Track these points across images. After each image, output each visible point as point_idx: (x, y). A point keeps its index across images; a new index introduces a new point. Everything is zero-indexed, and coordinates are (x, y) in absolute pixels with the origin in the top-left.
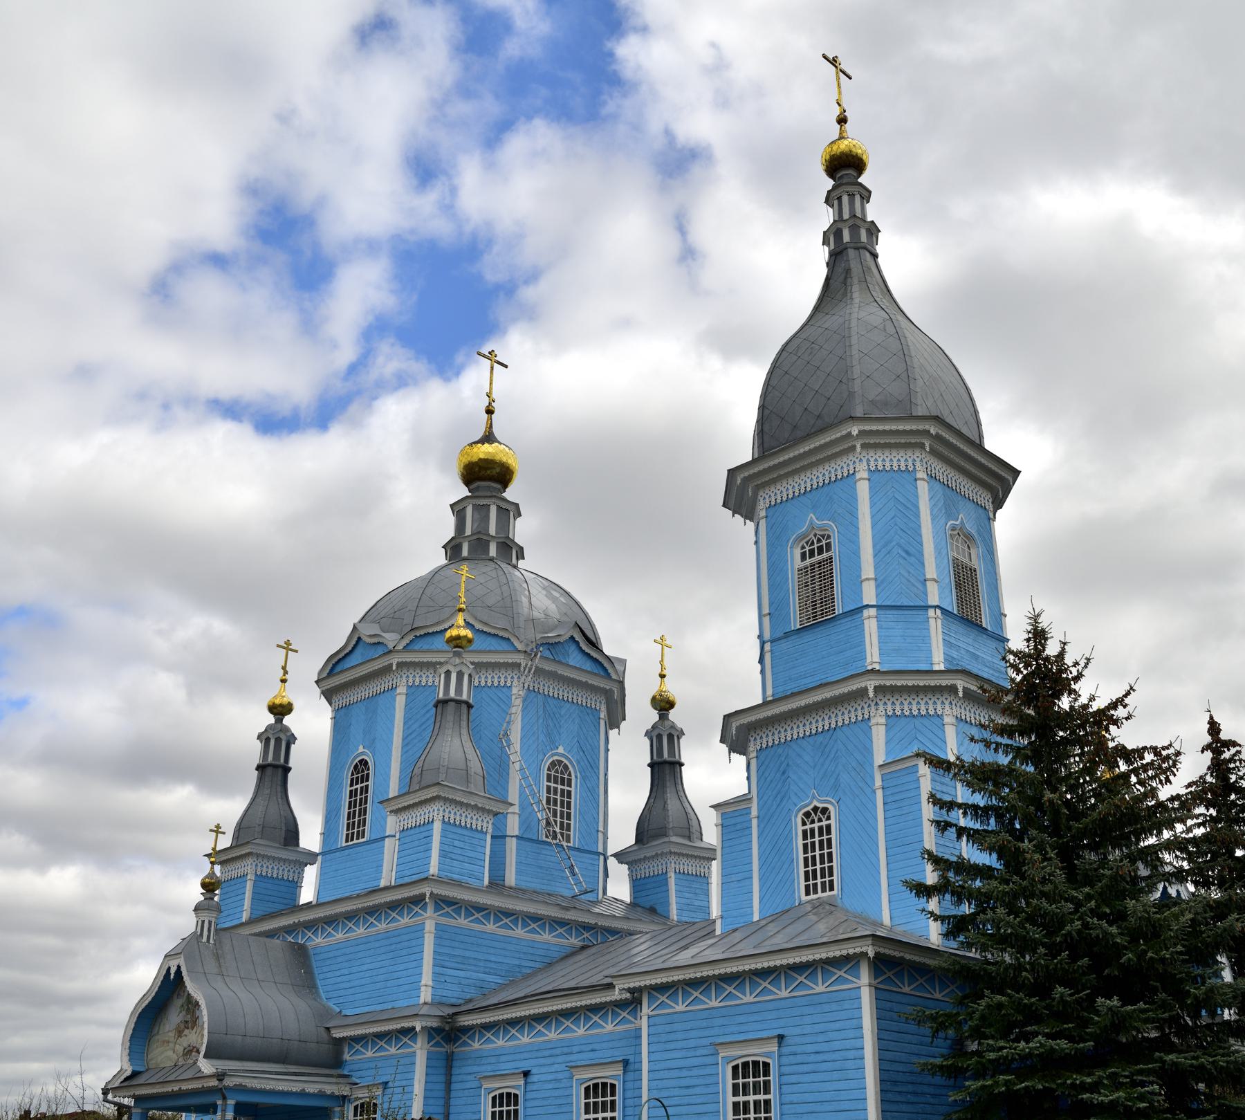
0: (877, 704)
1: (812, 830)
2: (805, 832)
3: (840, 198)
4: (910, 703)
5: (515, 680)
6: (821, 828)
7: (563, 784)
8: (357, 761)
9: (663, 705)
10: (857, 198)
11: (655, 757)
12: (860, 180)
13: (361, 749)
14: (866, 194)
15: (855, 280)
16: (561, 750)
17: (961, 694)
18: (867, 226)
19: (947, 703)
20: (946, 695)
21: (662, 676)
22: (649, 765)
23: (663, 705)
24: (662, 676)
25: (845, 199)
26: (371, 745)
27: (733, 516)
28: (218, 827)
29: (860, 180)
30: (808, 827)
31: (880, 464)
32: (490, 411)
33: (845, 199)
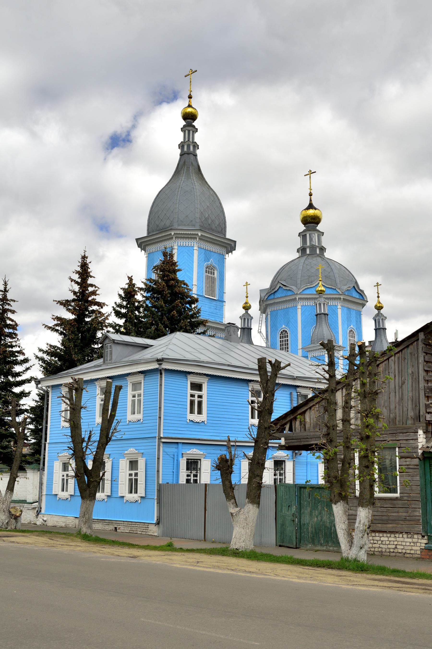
0: (299, 302)
1: (283, 340)
2: (281, 341)
3: (185, 131)
4: (335, 302)
5: (338, 303)
6: (285, 340)
7: (353, 338)
8: (282, 330)
9: (379, 308)
10: (191, 132)
11: (377, 327)
12: (193, 124)
13: (284, 326)
14: (195, 130)
15: (186, 167)
16: (352, 326)
17: (342, 300)
18: (193, 144)
19: (338, 302)
20: (338, 300)
21: (247, 297)
22: (375, 329)
23: (379, 308)
24: (247, 297)
25: (187, 132)
26: (287, 325)
27: (141, 251)
28: (377, 283)
29: (193, 124)
30: (282, 339)
31: (182, 244)
32: (311, 195)
33: (187, 132)
